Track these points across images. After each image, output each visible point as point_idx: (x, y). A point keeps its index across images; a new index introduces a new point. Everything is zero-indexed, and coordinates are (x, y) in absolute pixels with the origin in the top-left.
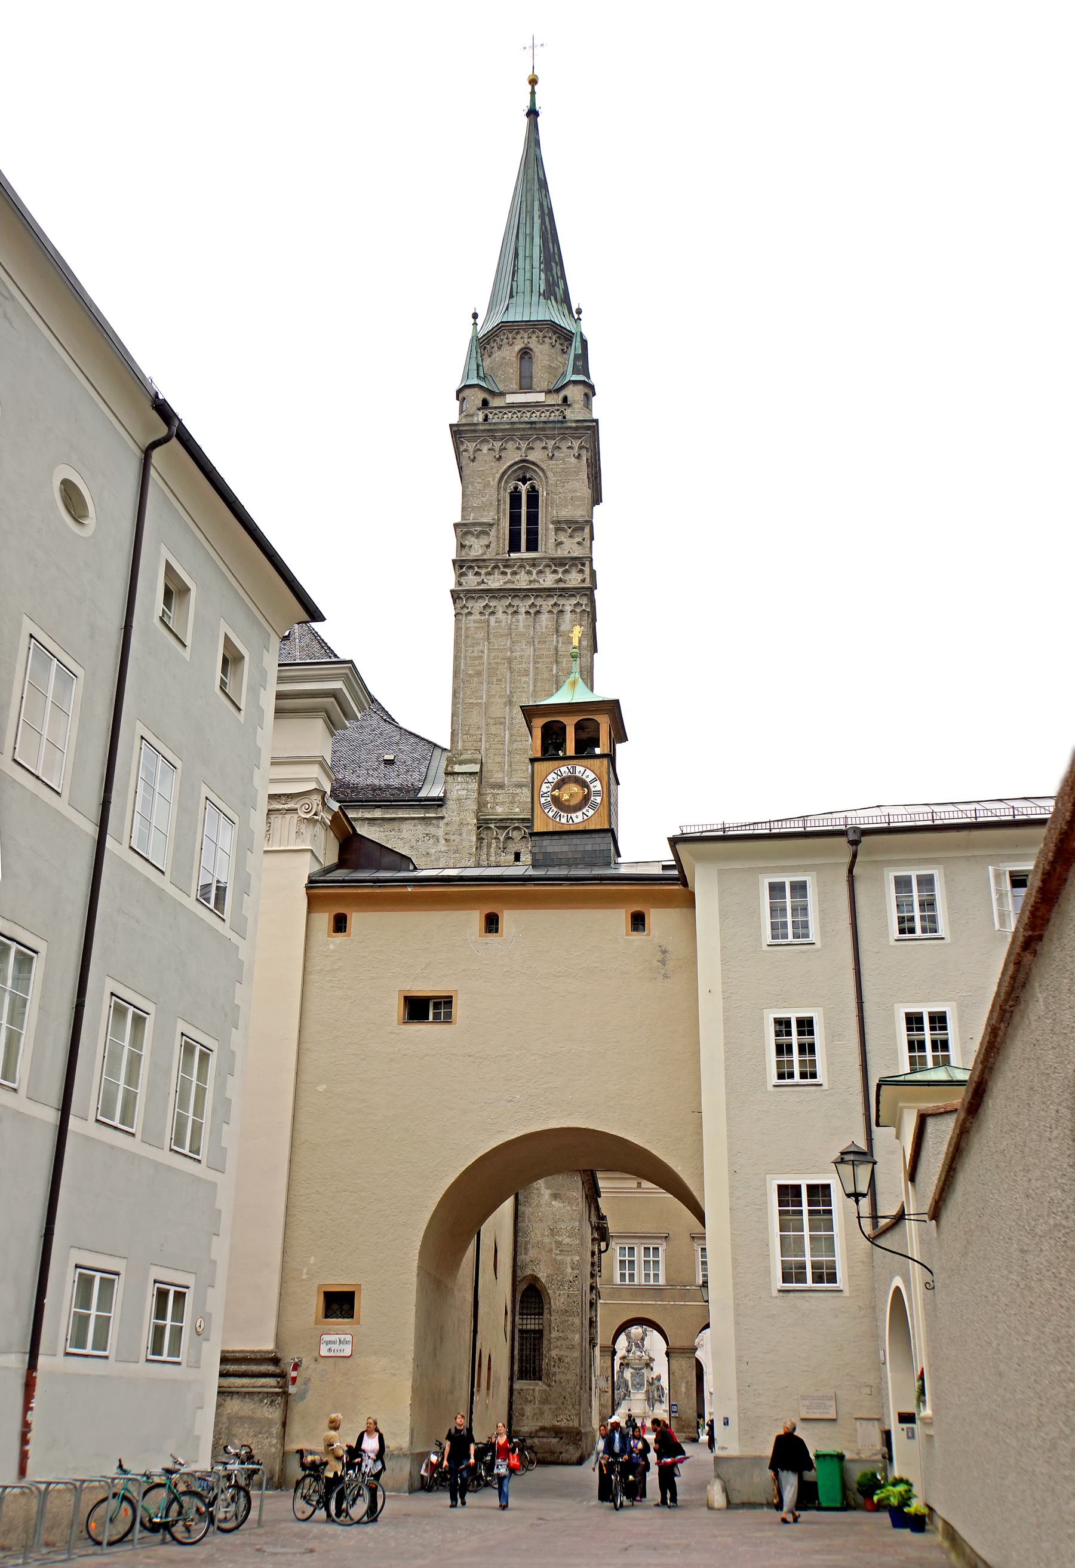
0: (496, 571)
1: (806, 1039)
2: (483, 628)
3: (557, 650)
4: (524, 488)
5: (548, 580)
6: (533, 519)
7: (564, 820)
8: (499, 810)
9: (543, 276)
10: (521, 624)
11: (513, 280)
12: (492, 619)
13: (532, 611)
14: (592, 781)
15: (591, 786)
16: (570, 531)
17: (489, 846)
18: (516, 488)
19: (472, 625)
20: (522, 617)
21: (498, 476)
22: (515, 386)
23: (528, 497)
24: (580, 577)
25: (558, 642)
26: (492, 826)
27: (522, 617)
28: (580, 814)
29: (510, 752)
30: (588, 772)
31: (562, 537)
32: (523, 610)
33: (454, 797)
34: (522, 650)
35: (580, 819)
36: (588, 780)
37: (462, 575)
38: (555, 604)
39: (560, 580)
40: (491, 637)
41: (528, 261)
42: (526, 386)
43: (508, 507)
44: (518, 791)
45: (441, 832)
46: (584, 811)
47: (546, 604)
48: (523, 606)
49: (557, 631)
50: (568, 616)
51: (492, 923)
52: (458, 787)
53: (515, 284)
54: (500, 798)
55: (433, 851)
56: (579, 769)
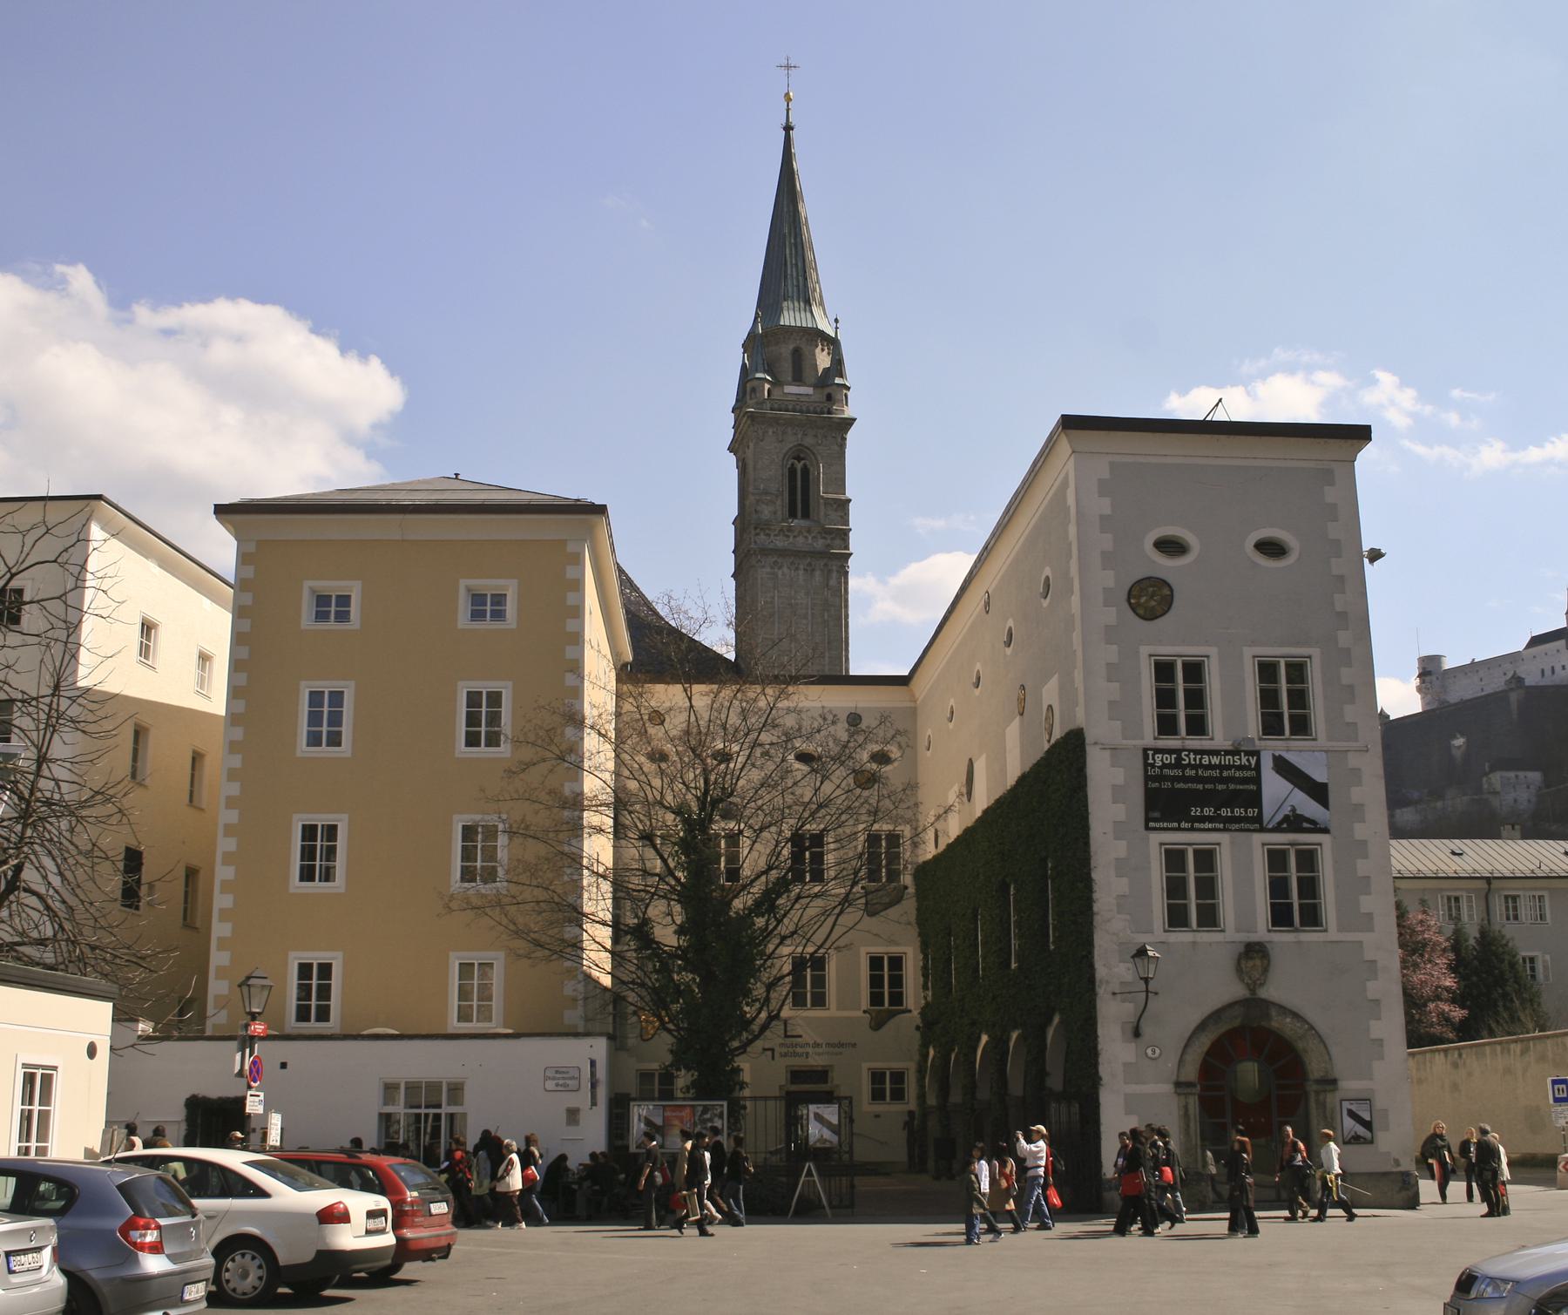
4: (799, 466)
51: (1375, 555)
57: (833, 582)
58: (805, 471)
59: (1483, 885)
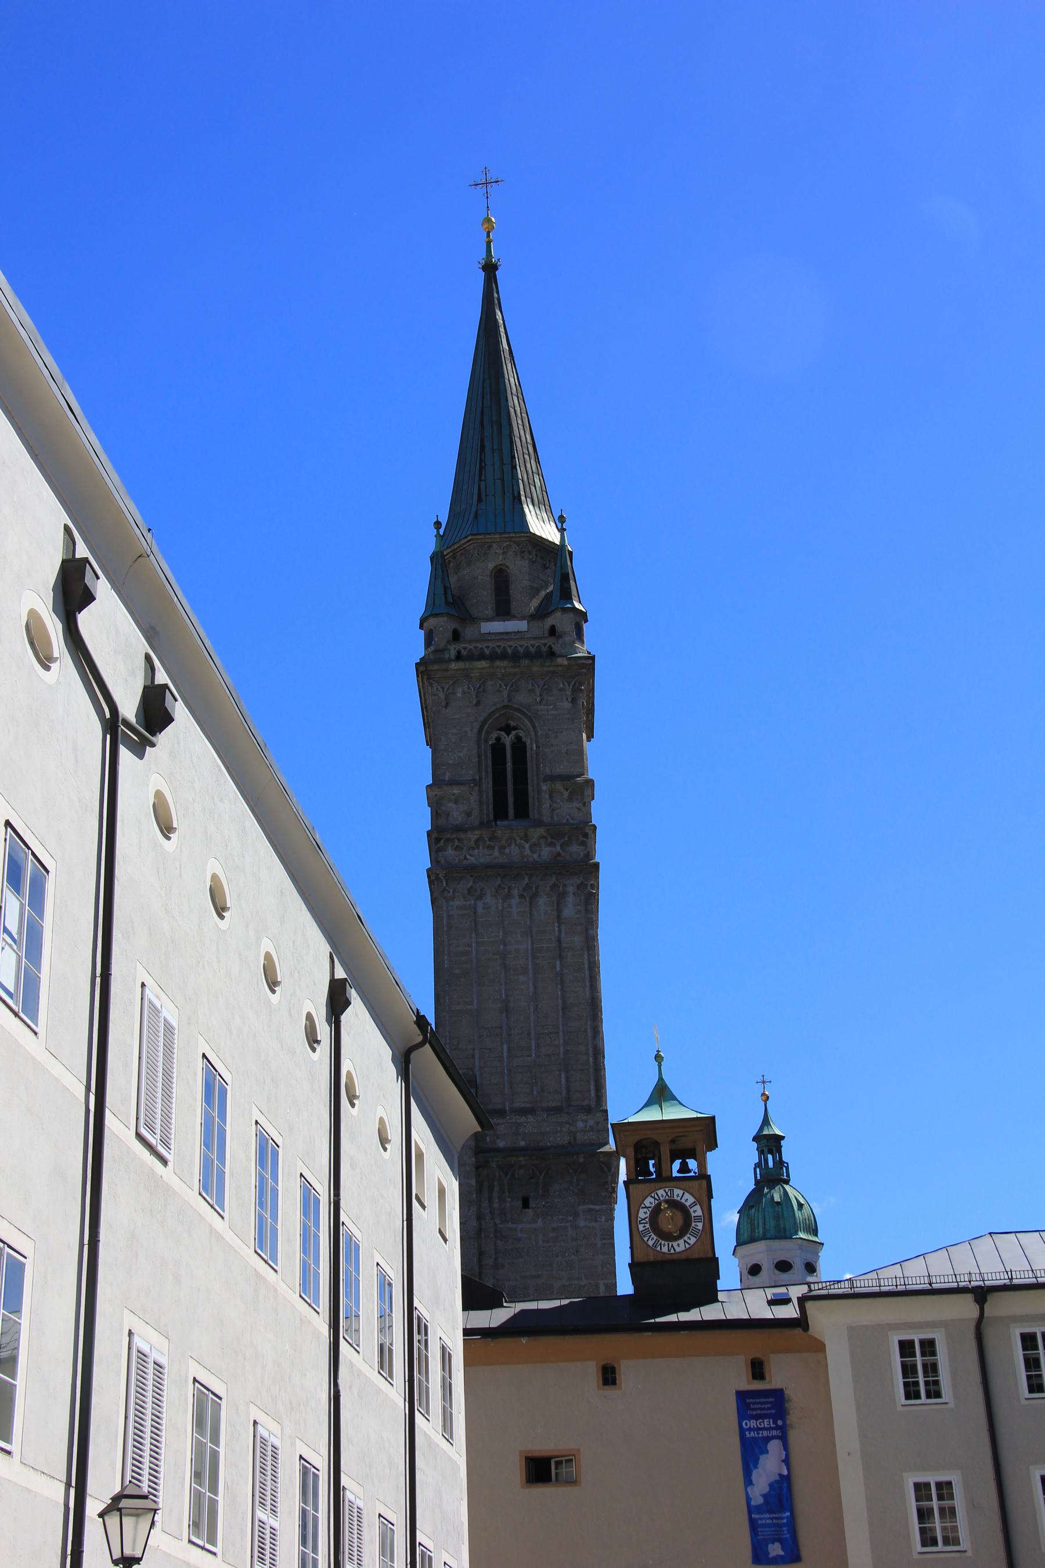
1: (946, 1503)
3: (559, 941)
4: (508, 740)
6: (521, 776)
7: (665, 1249)
11: (480, 480)
12: (480, 904)
14: (692, 1206)
15: (691, 1210)
17: (491, 1189)
18: (498, 739)
20: (515, 901)
21: (477, 726)
22: (490, 612)
25: (560, 932)
28: (681, 1242)
29: (510, 1071)
30: (687, 1195)
32: (515, 892)
35: (682, 1248)
36: (687, 1204)
37: (438, 850)
41: (496, 454)
42: (503, 611)
43: (490, 762)
44: (523, 1119)
46: (686, 1238)
49: (559, 917)
51: (609, 1376)
53: (483, 484)
56: (677, 1191)
57: (569, 911)
58: (519, 747)
59: (966, 1309)
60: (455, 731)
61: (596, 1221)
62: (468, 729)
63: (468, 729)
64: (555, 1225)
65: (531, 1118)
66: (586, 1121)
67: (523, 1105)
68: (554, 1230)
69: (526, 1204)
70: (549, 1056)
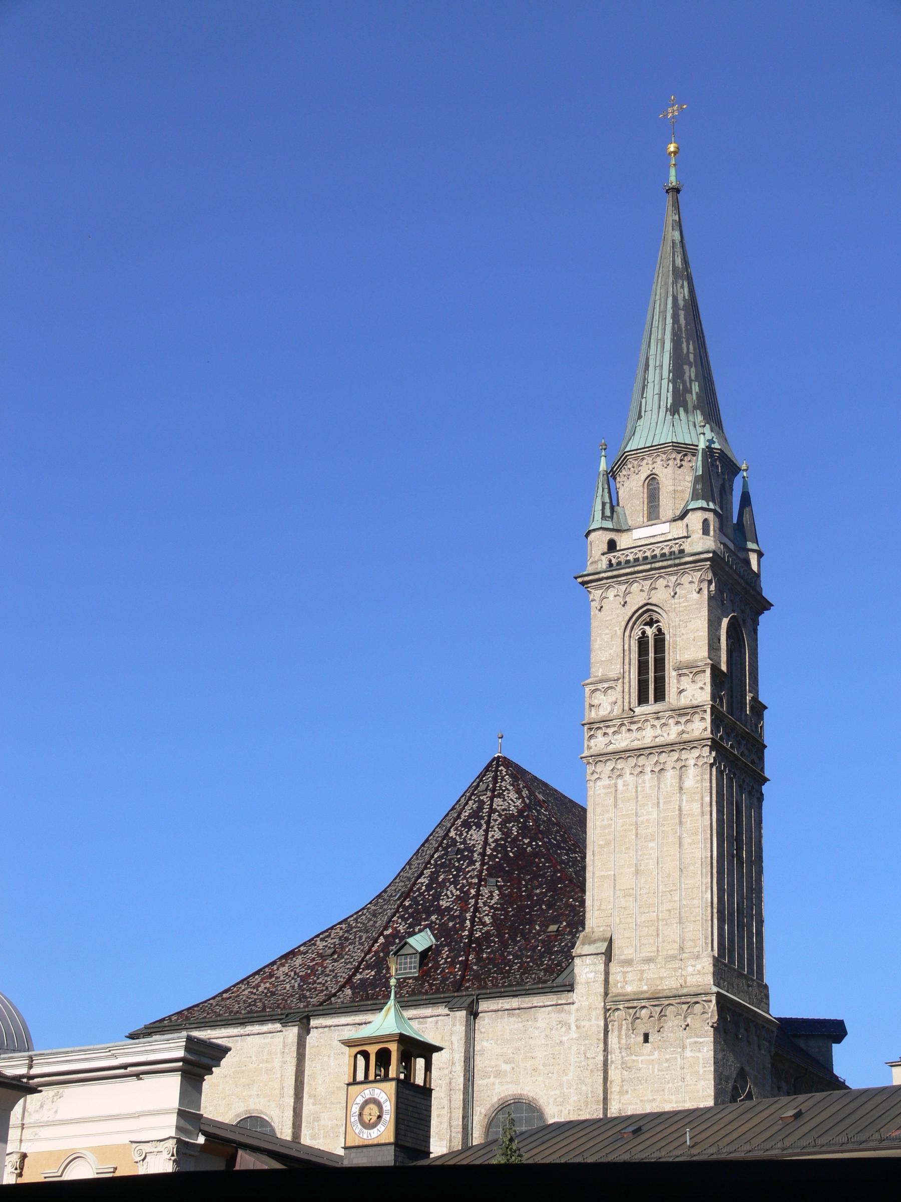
0: (624, 728)
2: (611, 793)
3: (680, 809)
5: (672, 733)
6: (660, 664)
7: (365, 1137)
8: (629, 989)
9: (671, 385)
10: (647, 785)
12: (620, 782)
13: (657, 770)
16: (691, 676)
19: (603, 791)
20: (648, 776)
22: (641, 518)
23: (656, 641)
24: (702, 725)
25: (681, 800)
26: (621, 1007)
27: (648, 776)
28: (375, 1130)
31: (685, 682)
32: (648, 769)
33: (583, 981)
34: (648, 813)
38: (678, 760)
39: (683, 732)
40: (619, 802)
41: (658, 371)
44: (646, 967)
45: (572, 1019)
47: (670, 759)
48: (648, 763)
49: (681, 788)
50: (692, 772)
52: (587, 970)
53: (644, 401)
54: (629, 976)
55: (565, 1039)
56: (377, 1091)
60: (607, 631)
61: (700, 1051)
62: (617, 629)
63: (617, 629)
64: (668, 1057)
65: (652, 965)
66: (694, 966)
67: (648, 955)
68: (667, 1060)
69: (646, 1038)
70: (669, 911)
